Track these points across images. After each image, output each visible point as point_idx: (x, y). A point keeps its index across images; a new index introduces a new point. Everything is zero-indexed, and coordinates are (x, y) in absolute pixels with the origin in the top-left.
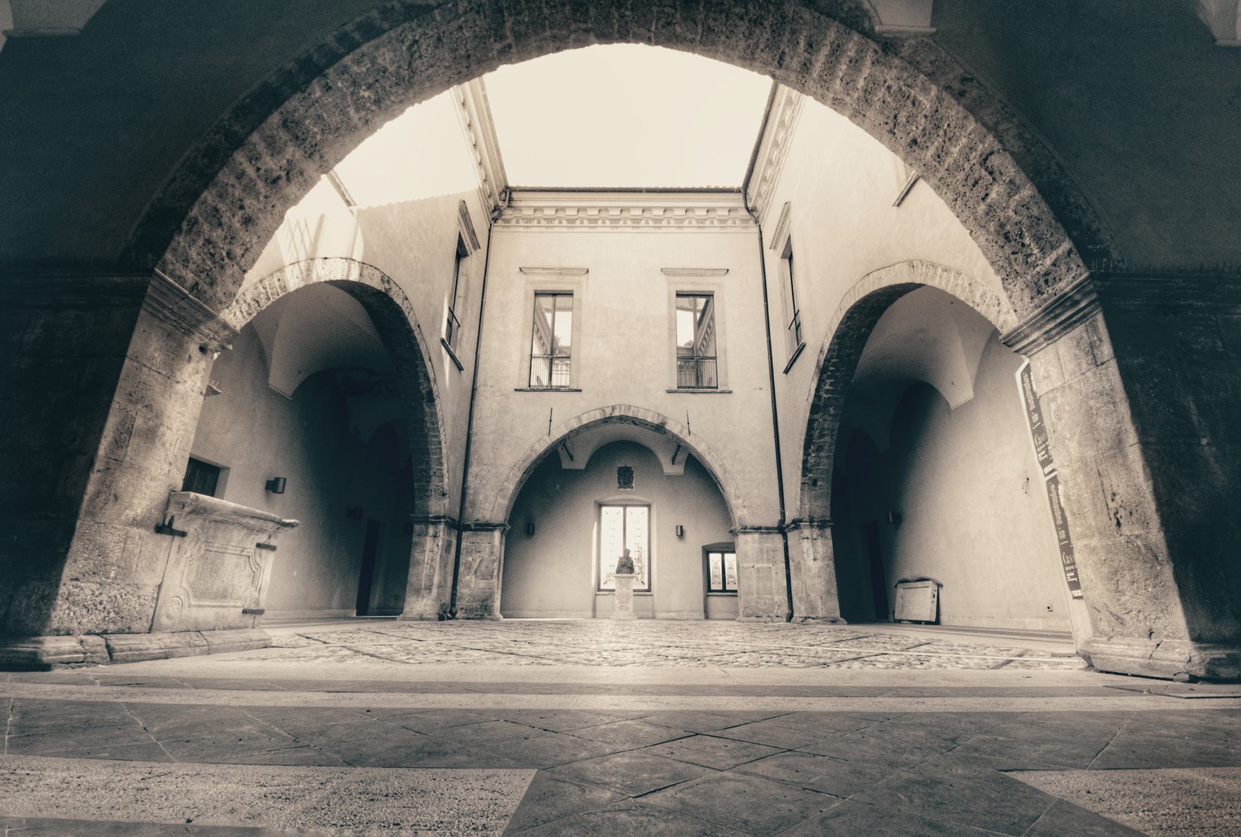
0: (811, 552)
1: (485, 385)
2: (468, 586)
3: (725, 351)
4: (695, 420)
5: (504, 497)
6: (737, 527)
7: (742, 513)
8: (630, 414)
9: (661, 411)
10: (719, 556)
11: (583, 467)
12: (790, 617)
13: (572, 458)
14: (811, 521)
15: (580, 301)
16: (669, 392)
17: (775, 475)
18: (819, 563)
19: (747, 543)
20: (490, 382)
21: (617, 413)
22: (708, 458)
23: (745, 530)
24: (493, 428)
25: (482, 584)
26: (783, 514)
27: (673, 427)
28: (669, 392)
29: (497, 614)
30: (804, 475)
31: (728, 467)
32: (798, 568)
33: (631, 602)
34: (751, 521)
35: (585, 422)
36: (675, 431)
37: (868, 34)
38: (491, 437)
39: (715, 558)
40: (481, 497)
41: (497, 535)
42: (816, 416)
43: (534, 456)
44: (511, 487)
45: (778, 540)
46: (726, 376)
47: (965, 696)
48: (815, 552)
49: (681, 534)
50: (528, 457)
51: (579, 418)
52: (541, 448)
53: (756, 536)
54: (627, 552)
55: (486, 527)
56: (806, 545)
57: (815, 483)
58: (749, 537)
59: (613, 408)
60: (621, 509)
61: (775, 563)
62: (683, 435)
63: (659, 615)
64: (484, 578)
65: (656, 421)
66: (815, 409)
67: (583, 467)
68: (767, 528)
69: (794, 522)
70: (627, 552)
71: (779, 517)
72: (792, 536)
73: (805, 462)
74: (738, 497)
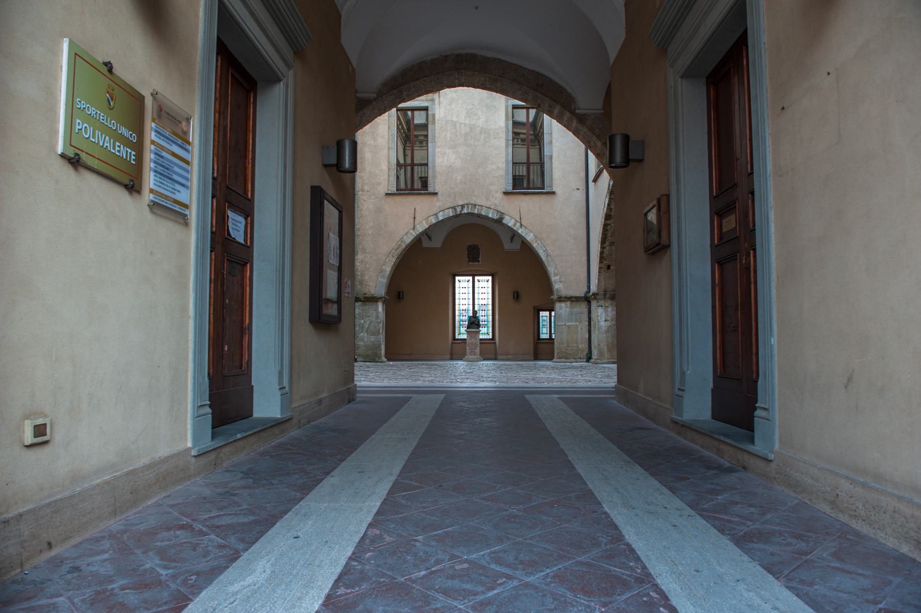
0: (603, 316)
1: (363, 190)
2: (362, 340)
3: (551, 158)
4: (525, 216)
5: (383, 277)
6: (555, 297)
7: (559, 287)
8: (476, 212)
9: (499, 209)
10: (547, 313)
11: (439, 246)
12: (589, 358)
13: (430, 238)
14: (605, 295)
15: (434, 115)
16: (506, 193)
17: (585, 258)
18: (608, 324)
19: (562, 308)
20: (366, 188)
21: (465, 211)
22: (535, 245)
23: (561, 299)
24: (371, 224)
25: (373, 338)
26: (589, 287)
27: (509, 221)
28: (506, 193)
29: (384, 359)
30: (601, 262)
31: (550, 252)
32: (595, 327)
33: (478, 349)
34: (564, 293)
35: (441, 218)
36: (510, 225)
37: (572, 112)
38: (370, 232)
39: (544, 315)
40: (366, 277)
41: (380, 307)
42: (608, 222)
43: (404, 246)
44: (388, 269)
45: (583, 307)
46: (551, 179)
47: (243, 331)
48: (607, 315)
49: (517, 296)
50: (400, 246)
51: (436, 215)
52: (408, 240)
53: (568, 303)
54: (475, 312)
55: (372, 300)
56: (600, 310)
57: (609, 267)
58: (563, 304)
59: (463, 206)
60: (470, 278)
61: (580, 322)
62: (517, 228)
63: (499, 357)
64: (373, 334)
65: (496, 217)
66: (608, 217)
67: (439, 246)
68: (576, 297)
69: (594, 294)
70: (475, 312)
71: (585, 289)
72: (594, 304)
73: (602, 253)
74: (556, 275)
